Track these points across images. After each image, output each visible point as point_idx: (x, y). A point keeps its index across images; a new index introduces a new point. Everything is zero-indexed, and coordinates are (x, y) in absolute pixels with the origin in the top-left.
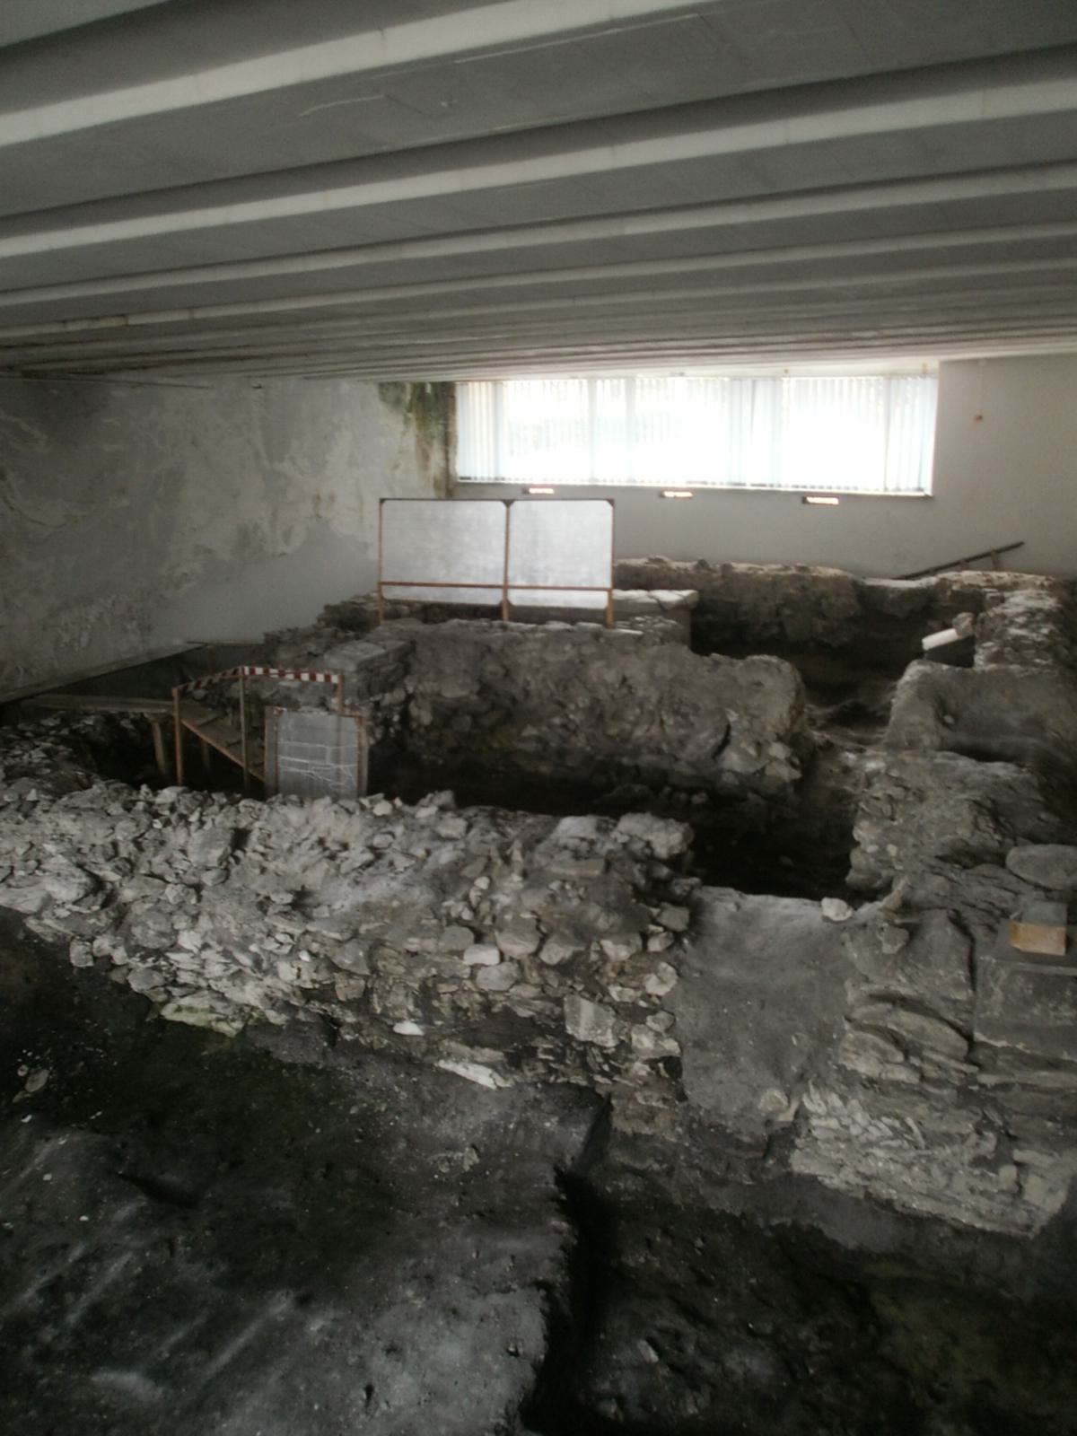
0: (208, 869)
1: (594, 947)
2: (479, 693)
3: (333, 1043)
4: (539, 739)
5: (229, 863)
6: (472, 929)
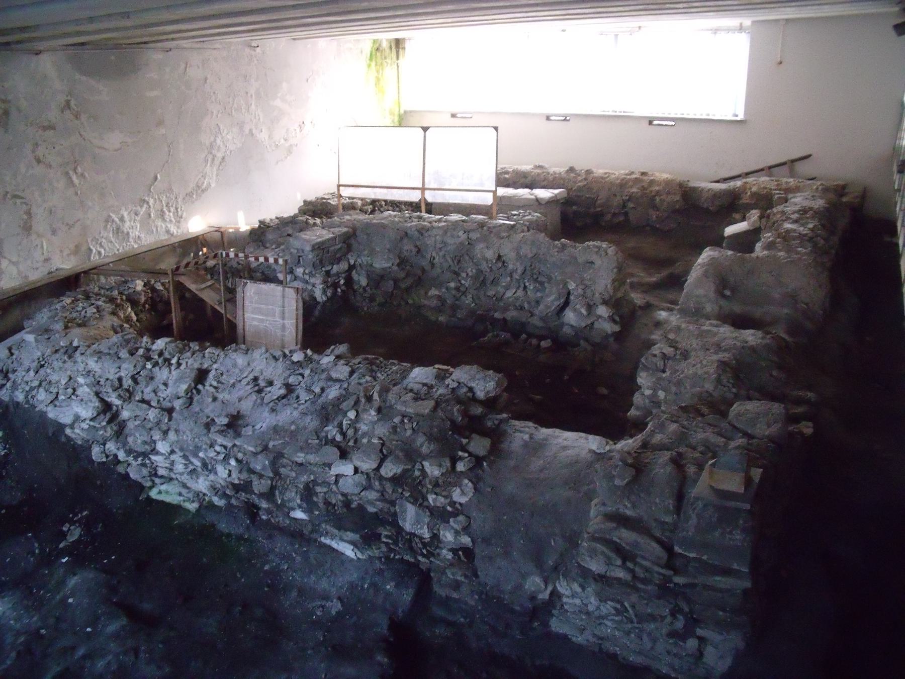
0: (179, 398)
1: (418, 466)
2: (398, 265)
4: (439, 298)
5: (192, 393)
6: (339, 448)
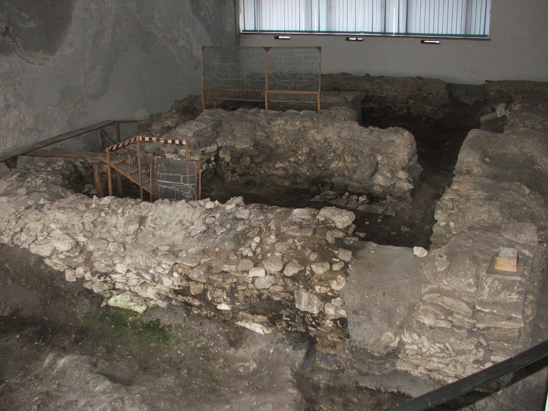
1: (308, 268)
3: (188, 315)
4: (284, 169)
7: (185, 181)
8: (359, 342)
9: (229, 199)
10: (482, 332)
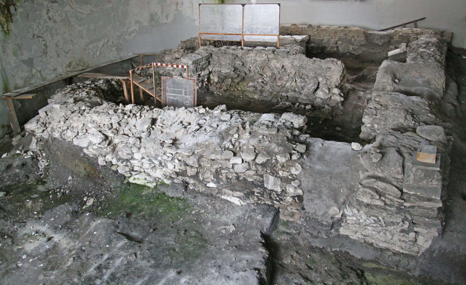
1: (274, 158)
6: (233, 151)
7: (186, 94)
8: (312, 214)
9: (216, 106)
10: (407, 209)
